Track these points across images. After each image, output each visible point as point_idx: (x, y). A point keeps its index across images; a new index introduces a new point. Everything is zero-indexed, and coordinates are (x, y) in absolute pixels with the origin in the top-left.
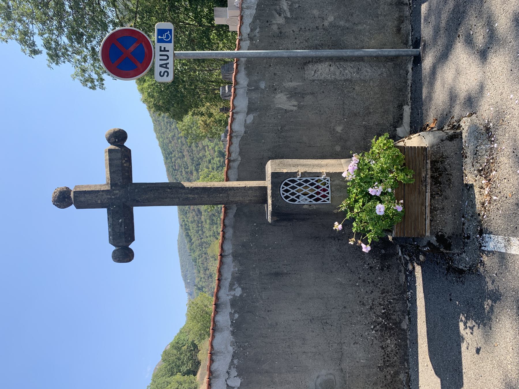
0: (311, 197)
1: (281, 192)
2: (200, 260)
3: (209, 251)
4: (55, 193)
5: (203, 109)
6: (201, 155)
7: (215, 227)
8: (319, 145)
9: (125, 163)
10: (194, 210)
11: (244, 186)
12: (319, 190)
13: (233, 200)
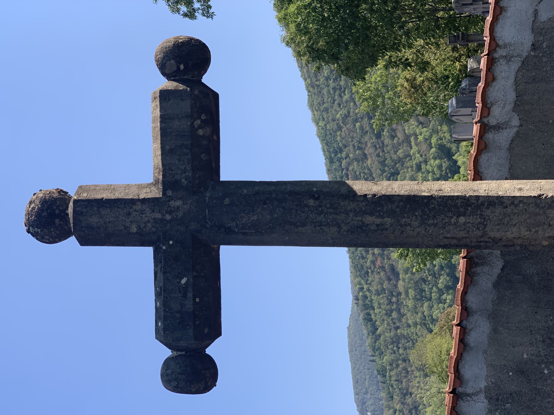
2: (393, 373)
3: (413, 356)
4: (31, 203)
5: (408, 54)
6: (400, 153)
7: (426, 304)
9: (200, 127)
10: (383, 268)
11: (534, 194)
13: (498, 235)
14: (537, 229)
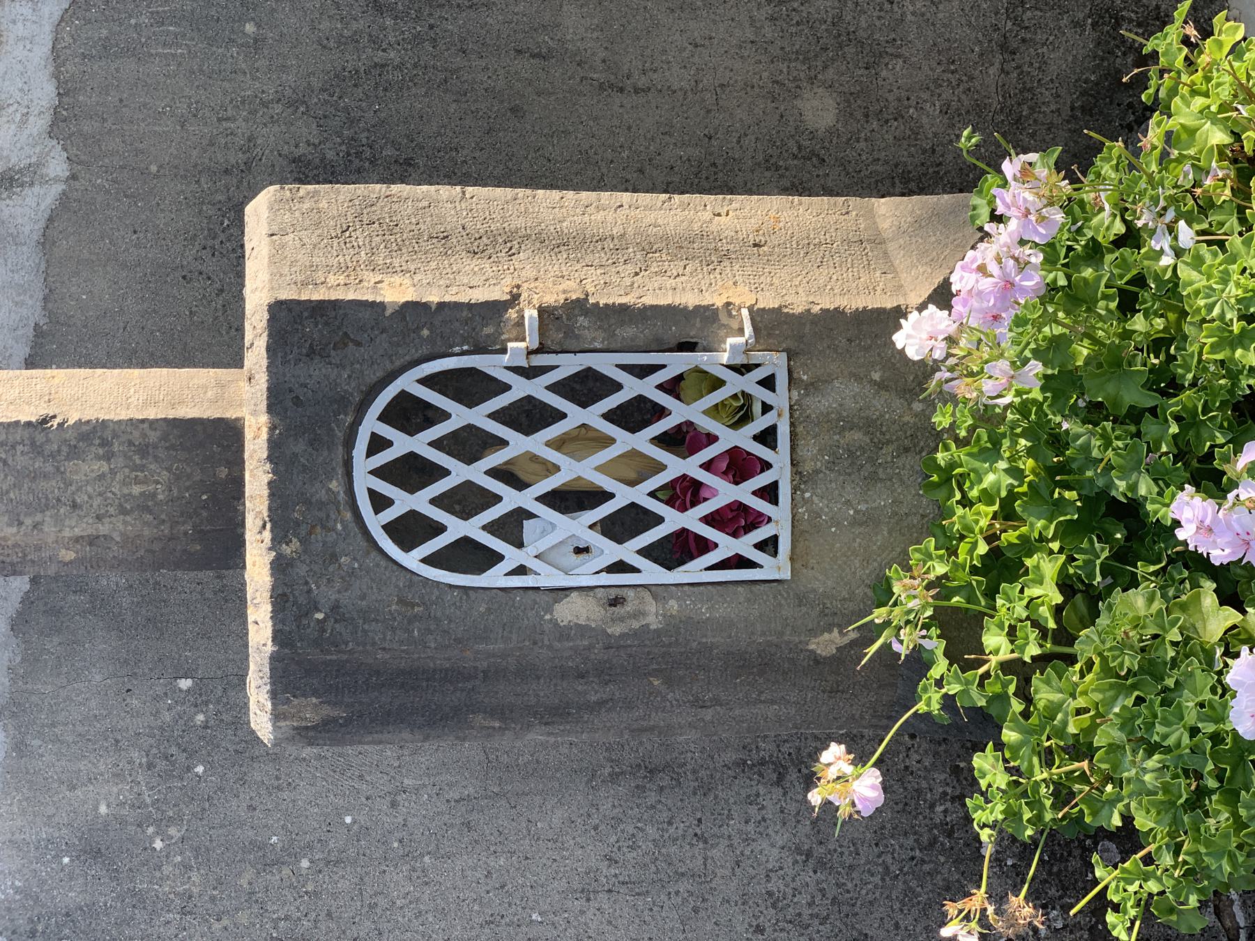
0: (625, 524)
1: (363, 481)
8: (678, 78)
12: (691, 466)
14: (39, 517)
